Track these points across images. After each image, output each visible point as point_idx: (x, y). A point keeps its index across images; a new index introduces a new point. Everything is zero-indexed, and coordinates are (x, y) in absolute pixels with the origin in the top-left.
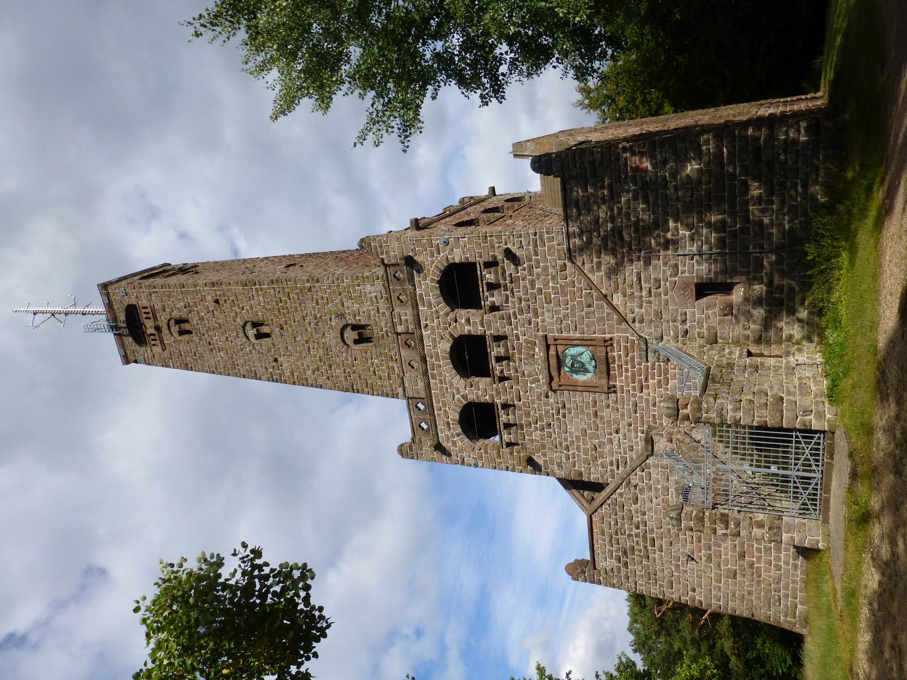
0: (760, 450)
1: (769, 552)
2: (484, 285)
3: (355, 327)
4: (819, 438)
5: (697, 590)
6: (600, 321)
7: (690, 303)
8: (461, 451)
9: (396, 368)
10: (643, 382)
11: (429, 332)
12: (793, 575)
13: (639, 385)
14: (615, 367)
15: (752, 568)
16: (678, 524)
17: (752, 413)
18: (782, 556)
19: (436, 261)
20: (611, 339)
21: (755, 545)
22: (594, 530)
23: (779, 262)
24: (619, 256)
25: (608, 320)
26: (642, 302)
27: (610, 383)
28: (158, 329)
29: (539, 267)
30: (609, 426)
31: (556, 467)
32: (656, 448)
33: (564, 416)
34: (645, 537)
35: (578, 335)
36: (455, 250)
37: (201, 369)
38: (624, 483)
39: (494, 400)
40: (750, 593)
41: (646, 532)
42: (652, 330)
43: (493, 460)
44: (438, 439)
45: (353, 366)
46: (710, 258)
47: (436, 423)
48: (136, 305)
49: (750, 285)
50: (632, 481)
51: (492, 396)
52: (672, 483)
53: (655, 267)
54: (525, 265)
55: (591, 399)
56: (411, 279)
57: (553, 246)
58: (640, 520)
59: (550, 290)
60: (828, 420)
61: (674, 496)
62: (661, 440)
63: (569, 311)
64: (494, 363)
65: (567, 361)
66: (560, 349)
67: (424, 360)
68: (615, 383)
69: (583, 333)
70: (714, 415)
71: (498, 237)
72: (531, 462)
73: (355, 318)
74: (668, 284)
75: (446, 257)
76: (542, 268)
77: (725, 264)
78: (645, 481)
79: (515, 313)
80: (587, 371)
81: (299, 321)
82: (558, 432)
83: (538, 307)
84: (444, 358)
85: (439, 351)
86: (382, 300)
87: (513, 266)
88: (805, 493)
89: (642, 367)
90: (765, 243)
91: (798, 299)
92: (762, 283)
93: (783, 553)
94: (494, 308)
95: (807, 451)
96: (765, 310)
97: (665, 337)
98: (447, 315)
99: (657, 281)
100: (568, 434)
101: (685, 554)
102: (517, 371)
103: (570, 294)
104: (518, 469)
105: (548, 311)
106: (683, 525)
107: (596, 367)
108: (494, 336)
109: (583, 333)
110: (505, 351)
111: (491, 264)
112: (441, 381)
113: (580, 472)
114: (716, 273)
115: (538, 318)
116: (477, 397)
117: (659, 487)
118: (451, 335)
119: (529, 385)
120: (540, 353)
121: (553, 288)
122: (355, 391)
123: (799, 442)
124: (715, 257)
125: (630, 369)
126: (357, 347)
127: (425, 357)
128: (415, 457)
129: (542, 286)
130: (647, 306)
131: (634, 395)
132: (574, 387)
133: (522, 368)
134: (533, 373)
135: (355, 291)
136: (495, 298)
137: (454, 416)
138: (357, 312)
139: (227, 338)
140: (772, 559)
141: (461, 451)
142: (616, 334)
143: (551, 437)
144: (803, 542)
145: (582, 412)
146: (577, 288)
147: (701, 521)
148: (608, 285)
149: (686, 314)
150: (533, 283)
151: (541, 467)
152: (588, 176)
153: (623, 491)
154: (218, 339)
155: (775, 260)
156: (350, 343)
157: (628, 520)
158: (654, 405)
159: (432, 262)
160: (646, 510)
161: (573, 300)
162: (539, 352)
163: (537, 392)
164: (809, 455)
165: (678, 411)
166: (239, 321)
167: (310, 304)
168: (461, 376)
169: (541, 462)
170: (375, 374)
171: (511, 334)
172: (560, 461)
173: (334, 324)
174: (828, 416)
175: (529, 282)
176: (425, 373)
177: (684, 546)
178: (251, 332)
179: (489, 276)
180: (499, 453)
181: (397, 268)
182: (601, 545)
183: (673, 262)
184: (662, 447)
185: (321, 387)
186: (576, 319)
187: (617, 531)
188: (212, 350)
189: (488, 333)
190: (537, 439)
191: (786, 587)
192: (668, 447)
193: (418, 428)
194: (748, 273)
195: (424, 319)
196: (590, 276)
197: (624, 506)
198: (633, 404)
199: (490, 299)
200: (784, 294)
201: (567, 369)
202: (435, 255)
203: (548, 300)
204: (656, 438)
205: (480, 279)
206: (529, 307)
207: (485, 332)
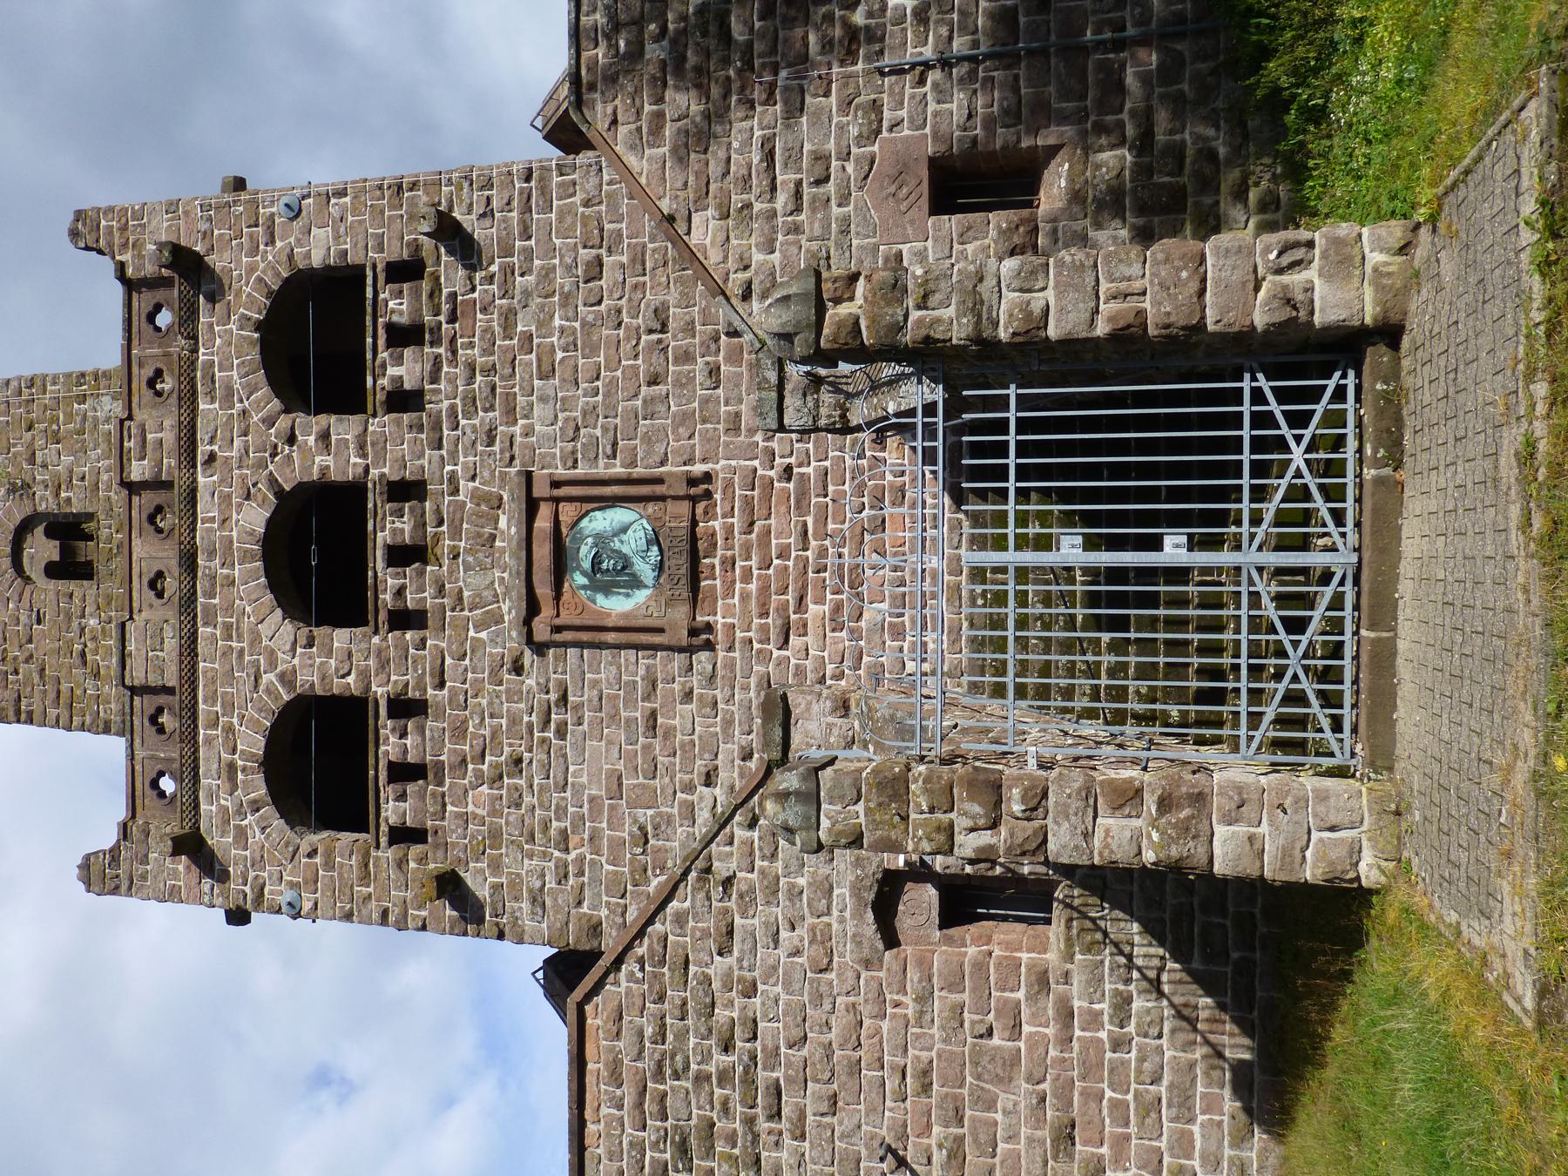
0: (1121, 624)
1: (1154, 1115)
2: (381, 332)
4: (1340, 393)
6: (682, 424)
7: (912, 222)
8: (259, 862)
10: (791, 609)
11: (215, 478)
13: (779, 622)
14: (713, 567)
16: (807, 818)
17: (1089, 280)
18: (1196, 1129)
19: (262, 265)
20: (707, 477)
21: (1108, 1094)
22: (590, 1066)
23: (1168, 72)
24: (715, 91)
25: (704, 421)
26: (774, 230)
27: (699, 618)
30: (689, 760)
31: (525, 905)
32: (796, 738)
33: (561, 733)
34: (749, 1081)
35: (618, 470)
36: (314, 231)
38: (693, 875)
39: (368, 688)
41: (754, 1058)
43: (347, 891)
44: (197, 821)
46: (972, 76)
47: (196, 769)
49: (1087, 151)
50: (716, 864)
51: (365, 675)
52: (842, 866)
53: (819, 117)
54: (494, 268)
55: (642, 672)
56: (188, 317)
58: (735, 1015)
59: (555, 339)
60: (1375, 270)
61: (847, 914)
62: (815, 707)
63: (600, 398)
64: (380, 565)
65: (584, 550)
66: (567, 512)
67: (189, 562)
68: (710, 619)
69: (633, 464)
70: (950, 312)
71: (432, 189)
72: (450, 886)
73: (57, 495)
74: (850, 168)
75: (288, 250)
76: (539, 275)
77: (1016, 89)
78: (758, 863)
80: (636, 583)
82: (541, 786)
83: (516, 389)
84: (246, 557)
85: (234, 534)
87: (461, 273)
89: (791, 563)
90: (1128, 18)
91: (1231, 177)
92: (1122, 143)
93: (1200, 1118)
94: (404, 400)
95: (1298, 456)
96: (1133, 228)
98: (270, 422)
99: (821, 158)
100: (568, 794)
101: (876, 1144)
102: (441, 591)
103: (607, 348)
104: (415, 918)
105: (543, 399)
106: (825, 823)
107: (660, 567)
108: (391, 484)
109: (633, 464)
111: (406, 271)
112: (228, 627)
113: (594, 921)
114: (989, 123)
115: (515, 422)
117: (802, 881)
118: (272, 481)
119: (471, 633)
120: (509, 528)
121: (562, 330)
122: (23, 717)
124: (986, 70)
125: (755, 572)
126: (52, 585)
128: (124, 888)
129: (533, 328)
130: (787, 243)
131: (764, 656)
133: (457, 580)
134: (485, 593)
135: (70, 417)
136: (405, 369)
137: (253, 742)
138: (64, 477)
140: (1163, 1144)
141: (259, 862)
142: (722, 462)
143: (518, 806)
144: (1297, 853)
145: (614, 716)
146: (627, 328)
147: (895, 797)
148: (679, 184)
150: (511, 317)
151: (482, 907)
153: (687, 904)
155: (1158, 67)
156: (34, 570)
157: (699, 1015)
158: (822, 680)
160: (756, 974)
161: (614, 365)
162: (507, 525)
163: (491, 654)
164: (1305, 471)
168: (289, 614)
169: (483, 893)
170: (85, 663)
172: (538, 884)
174: (1375, 258)
175: (500, 315)
176: (188, 602)
177: (876, 1110)
179: (398, 306)
180: (366, 865)
184: (818, 735)
186: (618, 421)
187: (660, 1065)
189: (374, 473)
190: (479, 811)
192: (836, 731)
193: (148, 791)
194: (1079, 117)
195: (207, 438)
196: (631, 160)
197: (687, 962)
199: (392, 371)
200: (1187, 171)
201: (580, 580)
202: (262, 247)
203: (546, 367)
204: (797, 701)
205: (369, 309)
206: (493, 389)
207: (367, 470)
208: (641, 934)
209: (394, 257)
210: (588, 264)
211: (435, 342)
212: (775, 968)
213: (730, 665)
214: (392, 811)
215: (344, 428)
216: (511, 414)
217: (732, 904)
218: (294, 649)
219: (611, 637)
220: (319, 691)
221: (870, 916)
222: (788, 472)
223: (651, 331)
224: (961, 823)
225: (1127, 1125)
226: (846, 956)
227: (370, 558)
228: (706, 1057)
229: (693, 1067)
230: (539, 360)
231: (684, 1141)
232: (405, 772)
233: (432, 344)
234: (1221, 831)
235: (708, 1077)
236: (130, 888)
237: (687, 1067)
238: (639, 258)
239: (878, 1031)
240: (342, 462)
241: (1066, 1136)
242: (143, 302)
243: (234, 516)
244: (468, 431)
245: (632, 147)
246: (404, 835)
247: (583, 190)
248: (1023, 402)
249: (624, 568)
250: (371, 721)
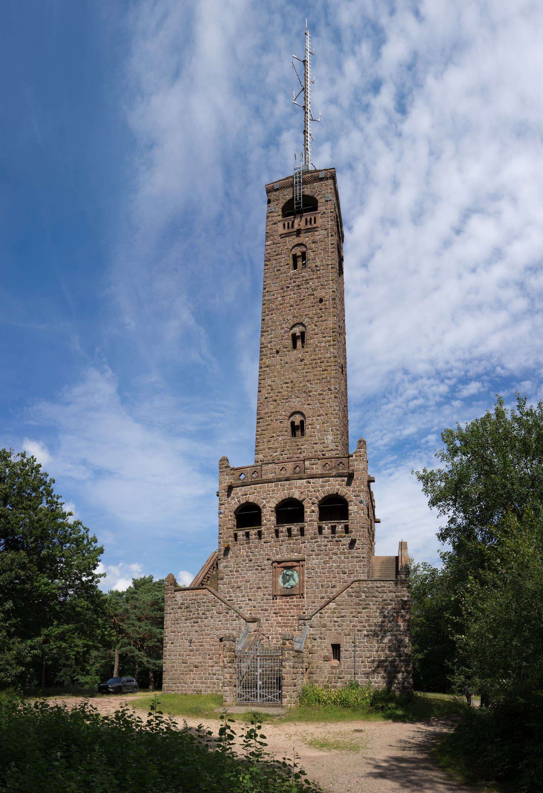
2: (334, 524)
3: (302, 422)
5: (173, 645)
9: (276, 454)
12: (189, 690)
15: (190, 671)
20: (304, 598)
24: (355, 607)
25: (314, 596)
26: (331, 618)
28: (298, 233)
29: (344, 558)
30: (252, 595)
31: (225, 564)
33: (257, 569)
34: (198, 618)
35: (306, 578)
36: (356, 507)
37: (267, 275)
39: (263, 526)
40: (176, 670)
42: (315, 622)
45: (276, 420)
48: (317, 210)
51: (266, 525)
55: (268, 585)
57: (356, 567)
64: (287, 527)
65: (290, 572)
66: (297, 568)
67: (287, 479)
69: (306, 582)
73: (310, 425)
79: (318, 542)
80: (284, 583)
81: (306, 376)
82: (246, 566)
84: (289, 493)
85: (293, 490)
86: (322, 447)
88: (274, 696)
94: (320, 529)
97: (312, 629)
98: (317, 498)
102: (283, 541)
103: (329, 575)
107: (287, 588)
108: (304, 528)
109: (306, 582)
110: (294, 534)
111: (347, 530)
112: (273, 491)
117: (228, 625)
118: (304, 499)
119: (275, 548)
122: (258, 421)
126: (289, 424)
127: (289, 480)
128: (221, 470)
132: (275, 576)
136: (327, 530)
137: (252, 499)
139: (292, 306)
143: (243, 561)
145: (260, 580)
146: (332, 580)
149: (324, 639)
152: (397, 593)
154: (292, 296)
156: (292, 419)
158: (267, 620)
159: (349, 491)
162: (295, 556)
165: (288, 640)
166: (306, 321)
167: (319, 388)
173: (305, 406)
178: (297, 330)
179: (340, 528)
181: (347, 466)
182: (189, 594)
183: (351, 633)
185: (259, 391)
187: (199, 603)
188: (282, 289)
189: (306, 524)
191: (182, 686)
193: (241, 472)
195: (314, 481)
198: (266, 609)
199: (326, 527)
204: (256, 624)
209: (349, 527)
211: (332, 537)
213: (270, 603)
214: (241, 533)
215: (315, 516)
216: (317, 555)
217: (224, 614)
218: (270, 507)
220: (262, 514)
224: (227, 658)
226: (218, 633)
227: (288, 524)
228: (201, 610)
231: (188, 608)
232: (247, 535)
236: (221, 472)
240: (308, 516)
241: (196, 667)
244: (314, 545)
246: (236, 536)
247: (360, 570)
250: (257, 527)
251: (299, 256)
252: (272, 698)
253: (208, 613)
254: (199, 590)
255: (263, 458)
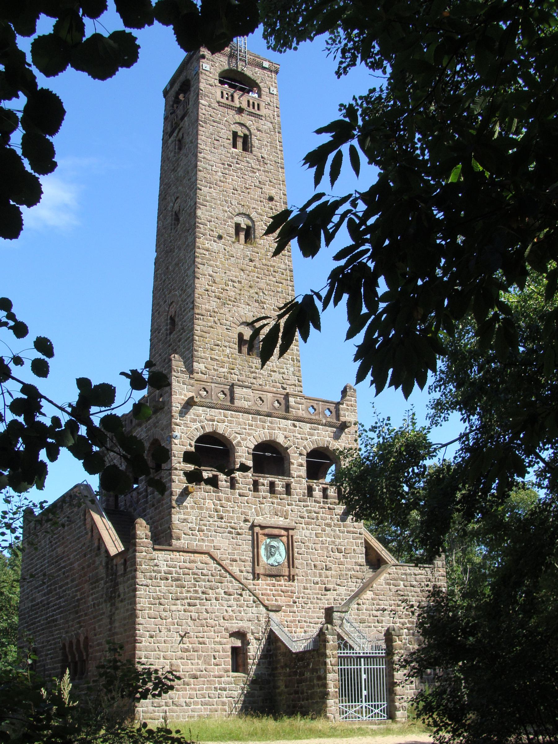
4: (384, 717)
5: (152, 639)
24: (394, 598)
25: (306, 580)
31: (182, 516)
33: (230, 532)
41: (202, 600)
55: (247, 558)
56: (330, 425)
64: (270, 479)
65: (276, 543)
79: (307, 506)
80: (268, 558)
82: (215, 525)
88: (381, 711)
93: (202, 707)
94: (310, 490)
98: (305, 448)
107: (272, 565)
116: (240, 456)
123: (381, 706)
127: (271, 417)
137: (221, 429)
141: (186, 425)
143: (209, 517)
162: (281, 521)
170: (215, 345)
171: (292, 500)
172: (189, 521)
188: (223, 164)
189: (292, 480)
190: (207, 504)
195: (300, 426)
199: (317, 488)
208: (226, 571)
210: (341, 549)
212: (223, 606)
215: (303, 471)
217: (236, 596)
218: (247, 447)
219: (256, 550)
221: (237, 630)
222: (295, 602)
223: (326, 566)
225: (199, 691)
226: (227, 624)
227: (273, 476)
229: (197, 583)
230: (320, 533)
233: (323, 501)
234: (333, 701)
235: (195, 587)
237: (197, 581)
238: (341, 564)
239: (211, 631)
241: (195, 677)
242: (332, 407)
243: (281, 432)
245: (385, 578)
248: (383, 668)
249: (272, 555)
251: (240, 137)
252: (379, 712)
253: (210, 591)
254: (196, 555)
255: (204, 369)
